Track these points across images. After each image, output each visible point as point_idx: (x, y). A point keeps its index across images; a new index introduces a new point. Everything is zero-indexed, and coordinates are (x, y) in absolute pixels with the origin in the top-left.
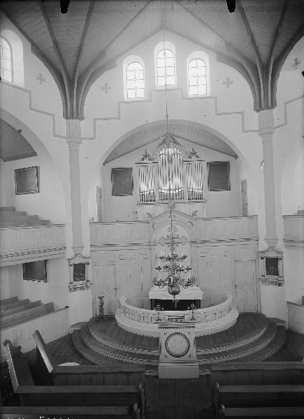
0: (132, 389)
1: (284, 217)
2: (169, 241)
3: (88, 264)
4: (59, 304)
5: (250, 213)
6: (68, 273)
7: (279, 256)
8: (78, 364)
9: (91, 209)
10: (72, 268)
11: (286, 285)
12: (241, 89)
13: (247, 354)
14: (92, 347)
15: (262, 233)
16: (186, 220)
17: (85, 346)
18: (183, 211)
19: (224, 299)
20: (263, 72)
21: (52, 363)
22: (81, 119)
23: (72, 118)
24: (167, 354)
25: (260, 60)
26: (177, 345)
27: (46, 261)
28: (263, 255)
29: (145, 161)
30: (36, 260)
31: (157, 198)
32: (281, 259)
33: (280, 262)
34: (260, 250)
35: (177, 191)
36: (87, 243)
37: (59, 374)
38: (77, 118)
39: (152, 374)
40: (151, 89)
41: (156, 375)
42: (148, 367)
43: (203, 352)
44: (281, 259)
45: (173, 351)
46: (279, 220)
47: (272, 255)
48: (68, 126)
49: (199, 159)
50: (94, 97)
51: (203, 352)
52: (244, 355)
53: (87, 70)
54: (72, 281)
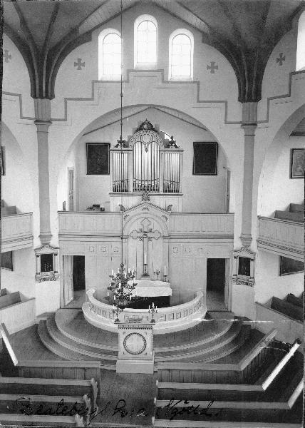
0: (85, 383)
1: (259, 218)
2: (141, 235)
3: (56, 255)
4: (25, 293)
5: (230, 211)
6: (57, 262)
7: (252, 257)
8: (242, 369)
9: (60, 194)
10: (39, 259)
11: (256, 286)
12: (227, 79)
13: (206, 351)
14: (57, 340)
15: (237, 234)
16: (161, 214)
17: (51, 338)
18: (158, 204)
19: (195, 296)
20: (38, 59)
21: (17, 357)
22: (51, 99)
23: (41, 97)
24: (126, 352)
25: (35, 46)
26: (135, 344)
27: (11, 252)
28: (237, 254)
29: (119, 148)
30: (295, 259)
31: (131, 189)
32: (253, 260)
33: (252, 263)
34: (235, 249)
35: (143, 182)
36: (55, 233)
37: (23, 367)
38: (47, 97)
39: (112, 369)
40: (131, 72)
41: (114, 369)
42: (105, 362)
43: (157, 350)
44: (253, 260)
45: (130, 349)
46: (255, 222)
47: (245, 255)
48: (36, 106)
49: (177, 149)
50: (67, 77)
51: (157, 350)
52: (201, 354)
53: (59, 44)
54: (39, 271)
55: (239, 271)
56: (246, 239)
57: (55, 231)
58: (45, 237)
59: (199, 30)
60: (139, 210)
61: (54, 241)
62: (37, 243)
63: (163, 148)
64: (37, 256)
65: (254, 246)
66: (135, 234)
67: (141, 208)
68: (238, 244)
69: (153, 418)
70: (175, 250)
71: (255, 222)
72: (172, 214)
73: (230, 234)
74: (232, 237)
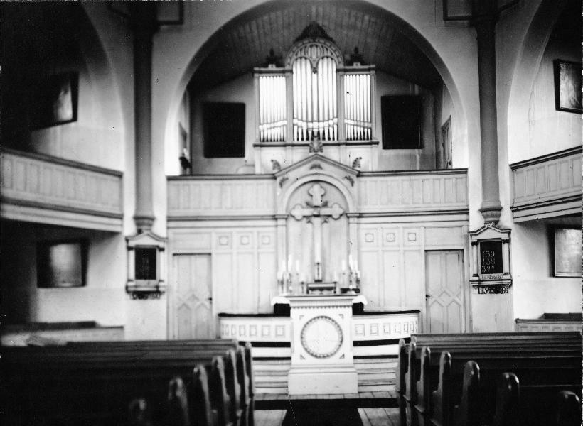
7: (505, 237)
10: (132, 254)
15: (475, 207)
28: (475, 239)
33: (505, 247)
55: (482, 269)
56: (492, 213)
57: (159, 212)
58: (143, 222)
59: (436, 101)
60: (304, 170)
61: (160, 228)
62: (128, 228)
63: (342, 66)
64: (129, 249)
65: (507, 219)
66: (298, 213)
67: (309, 165)
68: (476, 221)
69: (435, 391)
70: (369, 237)
71: (505, 173)
72: (360, 175)
73: (461, 206)
74: (466, 212)
